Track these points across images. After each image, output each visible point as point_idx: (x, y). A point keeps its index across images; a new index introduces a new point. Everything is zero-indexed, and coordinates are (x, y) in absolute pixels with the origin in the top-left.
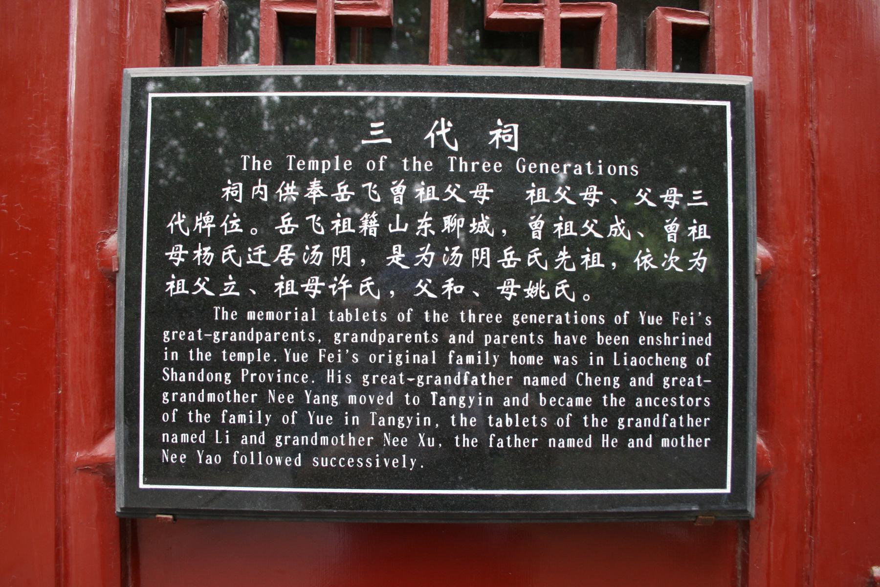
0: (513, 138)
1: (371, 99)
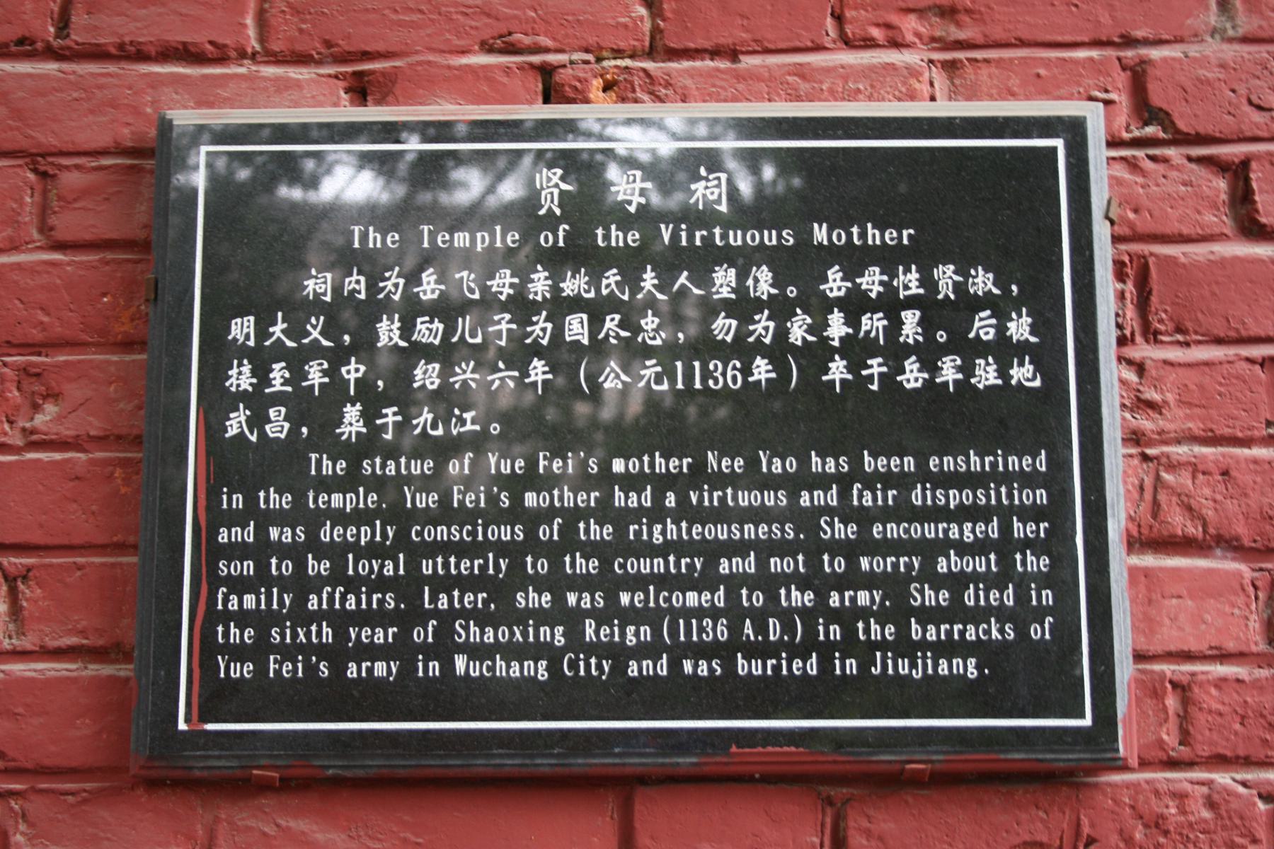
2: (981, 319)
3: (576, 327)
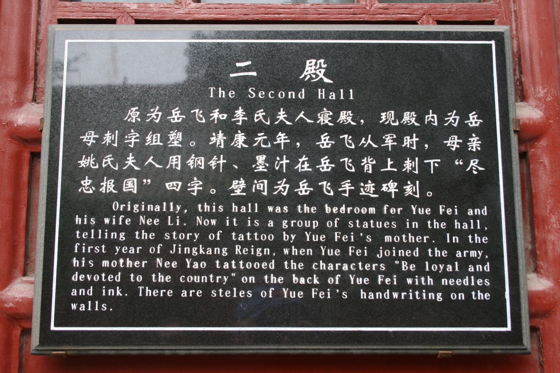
1: (60, 73)
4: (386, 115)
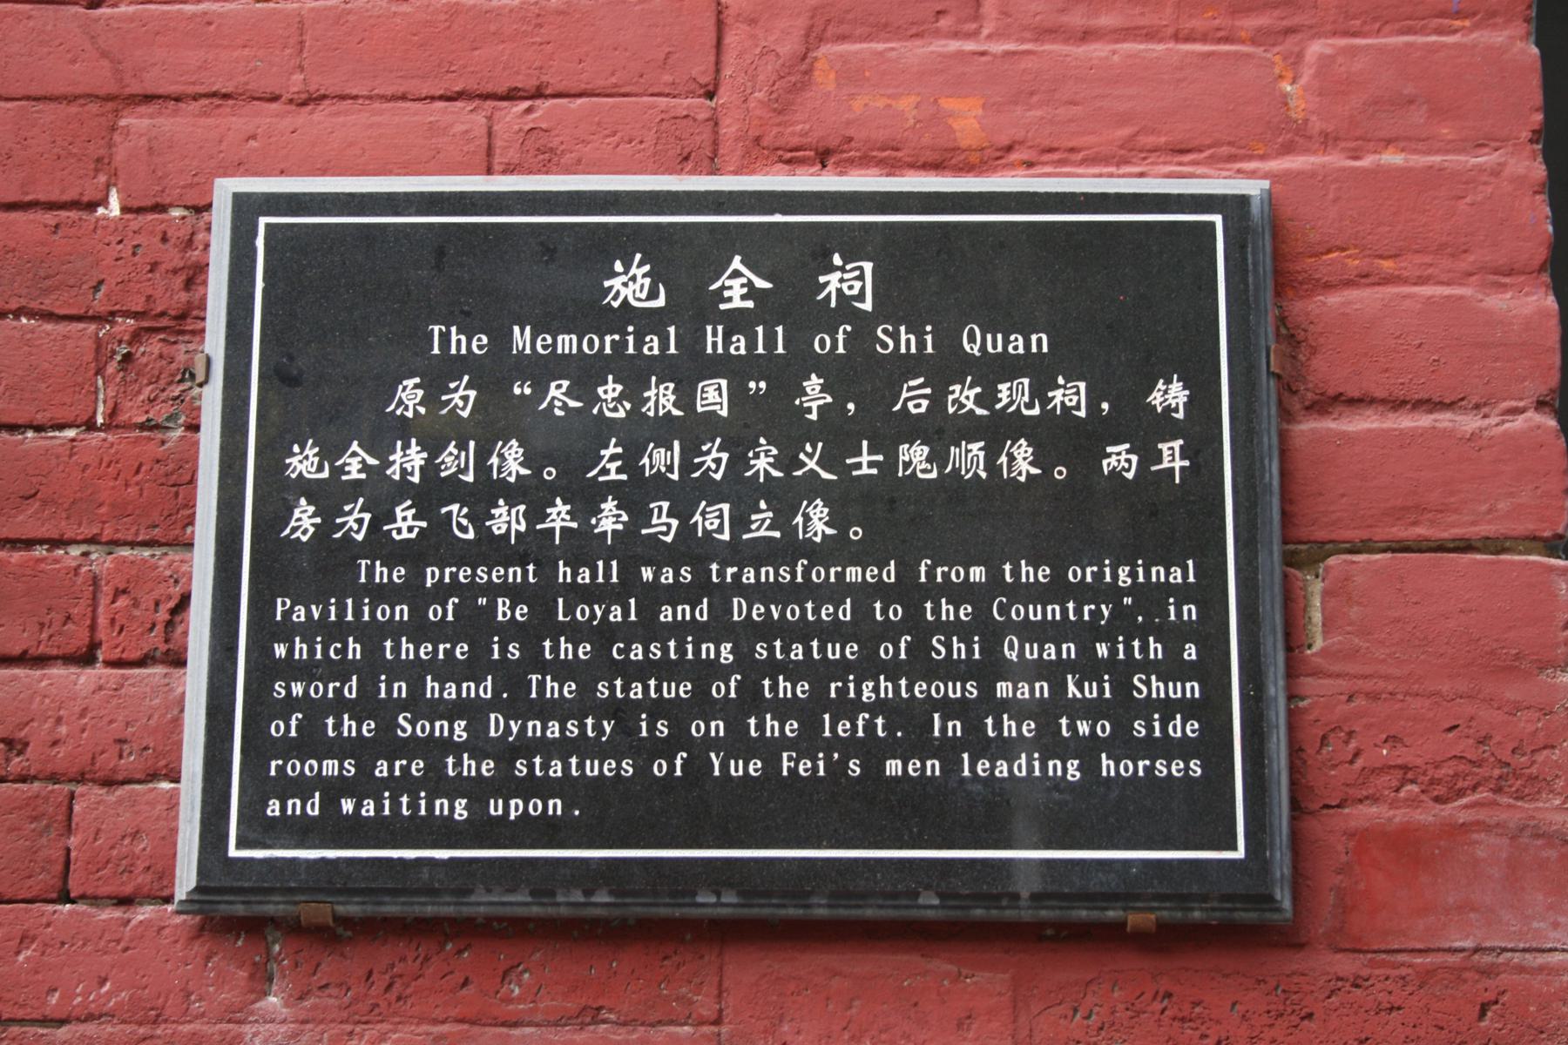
0: (863, 288)
2: (910, 389)
3: (712, 395)
4: (1010, 389)
